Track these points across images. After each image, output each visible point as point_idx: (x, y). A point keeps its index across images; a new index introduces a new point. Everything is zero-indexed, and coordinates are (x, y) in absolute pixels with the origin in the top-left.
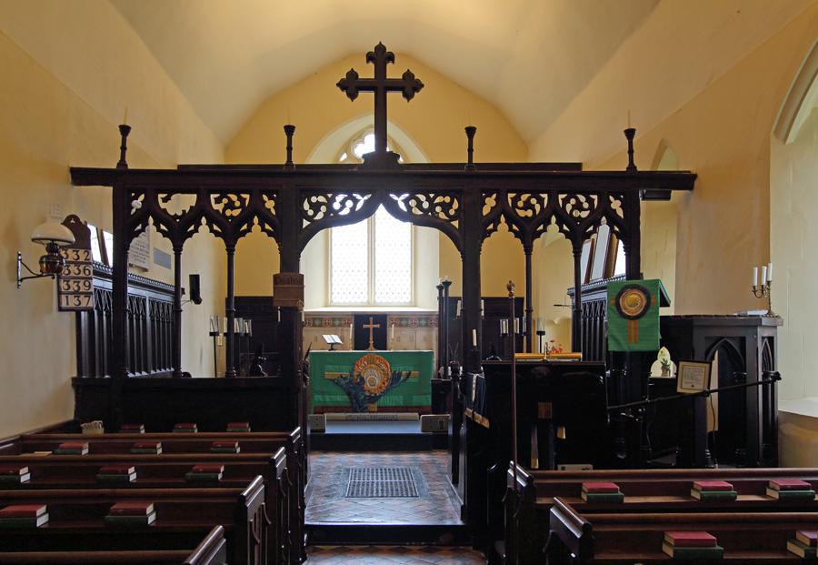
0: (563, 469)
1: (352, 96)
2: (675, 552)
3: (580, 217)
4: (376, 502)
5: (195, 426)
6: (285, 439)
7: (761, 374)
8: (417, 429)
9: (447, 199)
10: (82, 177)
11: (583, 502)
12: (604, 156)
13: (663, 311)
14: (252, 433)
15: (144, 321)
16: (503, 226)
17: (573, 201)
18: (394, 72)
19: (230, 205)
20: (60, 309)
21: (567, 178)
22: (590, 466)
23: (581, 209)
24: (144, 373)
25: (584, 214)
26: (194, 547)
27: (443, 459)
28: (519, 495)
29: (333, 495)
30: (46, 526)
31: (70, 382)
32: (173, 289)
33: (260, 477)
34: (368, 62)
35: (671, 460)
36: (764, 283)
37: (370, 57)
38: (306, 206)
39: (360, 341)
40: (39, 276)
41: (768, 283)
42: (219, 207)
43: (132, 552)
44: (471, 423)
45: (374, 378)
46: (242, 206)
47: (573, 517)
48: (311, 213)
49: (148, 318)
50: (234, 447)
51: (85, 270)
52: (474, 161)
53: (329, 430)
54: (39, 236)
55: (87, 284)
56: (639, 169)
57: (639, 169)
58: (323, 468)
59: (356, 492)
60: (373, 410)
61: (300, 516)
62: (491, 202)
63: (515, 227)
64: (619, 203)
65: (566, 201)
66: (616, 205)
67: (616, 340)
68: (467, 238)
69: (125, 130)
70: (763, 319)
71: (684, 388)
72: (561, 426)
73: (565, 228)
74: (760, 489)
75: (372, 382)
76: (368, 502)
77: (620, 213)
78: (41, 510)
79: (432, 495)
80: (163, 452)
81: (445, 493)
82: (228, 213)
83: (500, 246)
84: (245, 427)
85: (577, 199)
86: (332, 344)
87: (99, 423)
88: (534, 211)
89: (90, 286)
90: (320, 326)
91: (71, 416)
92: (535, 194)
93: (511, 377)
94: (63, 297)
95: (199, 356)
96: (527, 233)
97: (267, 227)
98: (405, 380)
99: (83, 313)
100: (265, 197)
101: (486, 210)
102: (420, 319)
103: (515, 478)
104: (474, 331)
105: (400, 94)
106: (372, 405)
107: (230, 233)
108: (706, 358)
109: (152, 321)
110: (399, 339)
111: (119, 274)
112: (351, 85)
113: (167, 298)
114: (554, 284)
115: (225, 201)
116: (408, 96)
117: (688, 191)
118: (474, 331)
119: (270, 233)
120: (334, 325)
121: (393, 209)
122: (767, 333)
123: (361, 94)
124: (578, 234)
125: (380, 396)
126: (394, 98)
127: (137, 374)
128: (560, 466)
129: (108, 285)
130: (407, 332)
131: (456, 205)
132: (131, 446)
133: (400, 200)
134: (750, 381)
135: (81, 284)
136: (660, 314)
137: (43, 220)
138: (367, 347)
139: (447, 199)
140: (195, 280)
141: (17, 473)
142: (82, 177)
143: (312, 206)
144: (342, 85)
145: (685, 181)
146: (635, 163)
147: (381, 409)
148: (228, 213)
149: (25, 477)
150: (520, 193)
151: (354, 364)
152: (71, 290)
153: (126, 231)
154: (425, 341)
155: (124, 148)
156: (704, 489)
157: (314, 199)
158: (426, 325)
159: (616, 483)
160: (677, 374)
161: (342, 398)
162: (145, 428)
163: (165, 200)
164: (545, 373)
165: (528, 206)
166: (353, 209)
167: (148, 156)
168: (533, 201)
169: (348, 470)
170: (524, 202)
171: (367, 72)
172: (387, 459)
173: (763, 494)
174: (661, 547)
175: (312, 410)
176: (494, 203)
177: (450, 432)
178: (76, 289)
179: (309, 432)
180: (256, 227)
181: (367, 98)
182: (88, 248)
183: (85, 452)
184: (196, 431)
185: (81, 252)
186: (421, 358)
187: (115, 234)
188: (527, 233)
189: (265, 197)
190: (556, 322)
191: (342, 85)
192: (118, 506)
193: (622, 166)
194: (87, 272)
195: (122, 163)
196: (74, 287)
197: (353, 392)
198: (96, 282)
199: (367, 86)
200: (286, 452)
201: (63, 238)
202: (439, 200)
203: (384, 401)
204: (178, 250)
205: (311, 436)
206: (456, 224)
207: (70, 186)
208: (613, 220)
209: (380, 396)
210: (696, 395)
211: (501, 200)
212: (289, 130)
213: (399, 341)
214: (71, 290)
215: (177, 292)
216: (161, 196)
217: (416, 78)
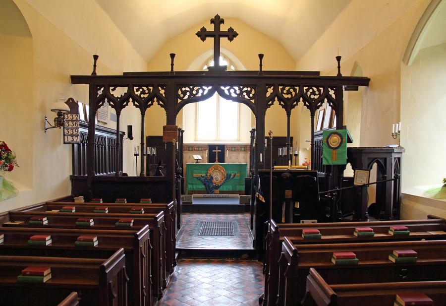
0: (303, 222)
1: (203, 39)
2: (336, 262)
3: (314, 98)
4: (213, 238)
5: (125, 200)
6: (165, 207)
7: (393, 175)
8: (237, 202)
9: (249, 89)
10: (76, 80)
11: (302, 239)
12: (327, 69)
13: (349, 145)
14: (152, 204)
15: (105, 148)
16: (276, 102)
17: (311, 91)
18: (224, 28)
19: (143, 92)
20: (65, 143)
21: (313, 79)
22: (316, 221)
23: (315, 94)
24: (105, 174)
25: (316, 97)
26: (108, 257)
27: (248, 216)
28: (272, 236)
29: (193, 235)
30: (51, 245)
31: (69, 178)
32: (116, 132)
33: (148, 225)
34: (211, 23)
35: (351, 218)
36: (397, 132)
37: (212, 21)
38: (180, 92)
39: (211, 159)
40: (54, 127)
41: (399, 132)
42: (138, 93)
43: (60, 258)
44: (258, 200)
45: (217, 177)
46: (149, 93)
47: (330, 246)
48: (182, 96)
49: (107, 147)
50: (141, 210)
51: (76, 124)
52: (263, 70)
53: (194, 203)
54: (54, 108)
55: (77, 131)
56: (343, 76)
57: (343, 75)
58: (190, 221)
59: (205, 233)
60: (216, 193)
61: (173, 245)
62: (270, 90)
63: (282, 103)
64: (333, 92)
65: (307, 90)
66: (332, 92)
67: (326, 159)
68: (259, 109)
69: (96, 57)
70: (395, 149)
71: (357, 183)
72: (297, 201)
73: (307, 103)
74: (386, 231)
75: (217, 179)
76: (209, 238)
77: (334, 96)
78: (48, 238)
79: (241, 235)
80: (109, 212)
81: (248, 234)
82: (142, 96)
83: (275, 114)
84: (149, 201)
85: (313, 89)
86: (197, 160)
87: (82, 197)
88: (292, 95)
89: (78, 132)
90: (192, 150)
91: (70, 194)
92: (292, 86)
93: (269, 178)
94: (66, 137)
95: (131, 167)
96: (288, 106)
97: (161, 103)
98: (233, 178)
99: (75, 145)
100: (160, 88)
101: (268, 95)
102: (241, 147)
103: (270, 226)
104: (261, 154)
105: (227, 38)
106: (217, 190)
107: (143, 106)
108: (368, 167)
109: (109, 148)
110: (231, 158)
111: (91, 126)
112: (203, 34)
113: (115, 137)
114: (304, 130)
115: (141, 90)
116: (231, 39)
117: (366, 87)
118: (261, 154)
119: (162, 106)
120: (199, 150)
121: (222, 94)
122: (397, 156)
123: (208, 38)
124: (313, 107)
125: (220, 186)
126: (224, 41)
127: (98, 174)
128: (301, 221)
129: (87, 131)
130: (234, 154)
131: (253, 92)
132: (94, 209)
133: (226, 89)
134: (388, 179)
135: (74, 131)
136: (347, 147)
137: (57, 101)
138: (214, 161)
139: (249, 89)
140: (130, 128)
141: (42, 220)
142: (76, 80)
143: (182, 92)
144: (198, 34)
145: (365, 82)
146: (341, 72)
147: (221, 192)
148: (142, 96)
149: (45, 222)
150: (285, 86)
151: (208, 170)
152: (69, 134)
153: (95, 104)
154: (243, 159)
155: (95, 66)
156: (360, 231)
157: (184, 89)
158: (244, 151)
159: (318, 229)
160: (354, 176)
161: (202, 187)
162: (103, 200)
163: (113, 90)
164: (288, 176)
165: (289, 92)
166: (202, 94)
167: (107, 69)
168: (291, 90)
169: (202, 222)
170: (287, 91)
171: (211, 28)
172: (222, 217)
173: (387, 233)
174: (331, 260)
175: (187, 193)
176: (272, 91)
177: (251, 204)
178: (72, 133)
179: (181, 203)
180: (155, 103)
181: (210, 41)
182: (77, 113)
183: (74, 211)
184: (126, 202)
185: (74, 116)
186: (241, 167)
187: (89, 105)
188: (288, 106)
189: (160, 88)
190: (308, 149)
191: (198, 34)
192: (81, 237)
193: (335, 74)
194: (77, 125)
195: (94, 73)
196: (71, 132)
197: (207, 184)
198: (81, 130)
199: (210, 35)
200: (164, 213)
201: (65, 109)
202: (245, 89)
203: (223, 188)
204: (118, 114)
205: (183, 206)
206: (253, 101)
207: (70, 85)
208: (330, 100)
209: (220, 186)
210: (361, 186)
211: (275, 90)
212: (173, 56)
213: (231, 158)
214: (69, 134)
215: (119, 135)
216: (111, 88)
217: (234, 31)
